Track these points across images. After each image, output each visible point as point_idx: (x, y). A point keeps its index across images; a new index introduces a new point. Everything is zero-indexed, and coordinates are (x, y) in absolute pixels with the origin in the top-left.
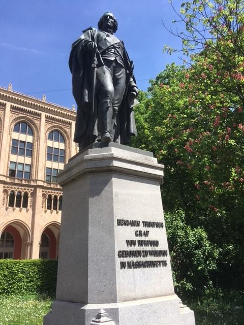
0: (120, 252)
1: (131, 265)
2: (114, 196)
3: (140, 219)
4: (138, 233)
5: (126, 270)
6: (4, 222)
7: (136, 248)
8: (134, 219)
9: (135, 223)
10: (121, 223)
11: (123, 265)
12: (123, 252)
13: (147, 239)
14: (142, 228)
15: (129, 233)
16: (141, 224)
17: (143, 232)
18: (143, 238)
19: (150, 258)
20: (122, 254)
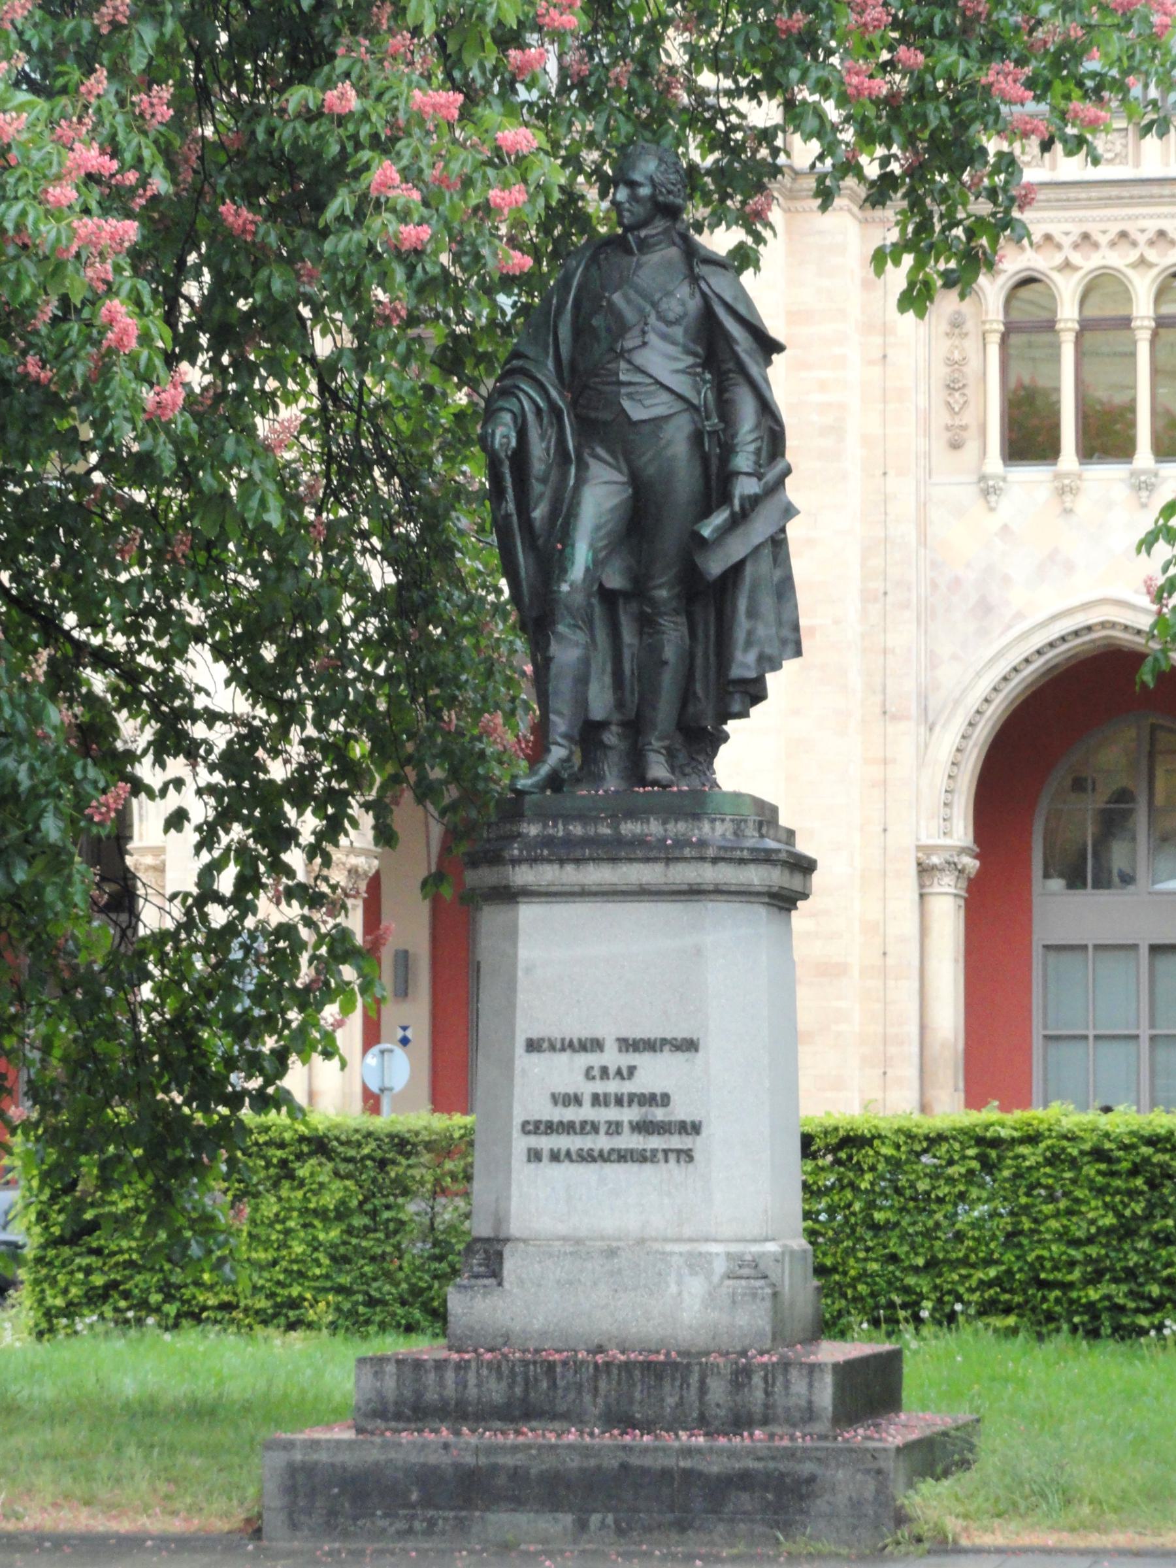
0: (526, 1123)
1: (555, 1157)
2: (520, 974)
3: (609, 1033)
4: (596, 1072)
5: (548, 1169)
6: (664, 1100)
7: (588, 1112)
8: (585, 1034)
9: (596, 1045)
10: (533, 1046)
11: (535, 1156)
12: (537, 1123)
13: (627, 1087)
14: (612, 1058)
15: (567, 1072)
16: (611, 1046)
17: (612, 1071)
18: (613, 1087)
19: (630, 1141)
20: (534, 1128)
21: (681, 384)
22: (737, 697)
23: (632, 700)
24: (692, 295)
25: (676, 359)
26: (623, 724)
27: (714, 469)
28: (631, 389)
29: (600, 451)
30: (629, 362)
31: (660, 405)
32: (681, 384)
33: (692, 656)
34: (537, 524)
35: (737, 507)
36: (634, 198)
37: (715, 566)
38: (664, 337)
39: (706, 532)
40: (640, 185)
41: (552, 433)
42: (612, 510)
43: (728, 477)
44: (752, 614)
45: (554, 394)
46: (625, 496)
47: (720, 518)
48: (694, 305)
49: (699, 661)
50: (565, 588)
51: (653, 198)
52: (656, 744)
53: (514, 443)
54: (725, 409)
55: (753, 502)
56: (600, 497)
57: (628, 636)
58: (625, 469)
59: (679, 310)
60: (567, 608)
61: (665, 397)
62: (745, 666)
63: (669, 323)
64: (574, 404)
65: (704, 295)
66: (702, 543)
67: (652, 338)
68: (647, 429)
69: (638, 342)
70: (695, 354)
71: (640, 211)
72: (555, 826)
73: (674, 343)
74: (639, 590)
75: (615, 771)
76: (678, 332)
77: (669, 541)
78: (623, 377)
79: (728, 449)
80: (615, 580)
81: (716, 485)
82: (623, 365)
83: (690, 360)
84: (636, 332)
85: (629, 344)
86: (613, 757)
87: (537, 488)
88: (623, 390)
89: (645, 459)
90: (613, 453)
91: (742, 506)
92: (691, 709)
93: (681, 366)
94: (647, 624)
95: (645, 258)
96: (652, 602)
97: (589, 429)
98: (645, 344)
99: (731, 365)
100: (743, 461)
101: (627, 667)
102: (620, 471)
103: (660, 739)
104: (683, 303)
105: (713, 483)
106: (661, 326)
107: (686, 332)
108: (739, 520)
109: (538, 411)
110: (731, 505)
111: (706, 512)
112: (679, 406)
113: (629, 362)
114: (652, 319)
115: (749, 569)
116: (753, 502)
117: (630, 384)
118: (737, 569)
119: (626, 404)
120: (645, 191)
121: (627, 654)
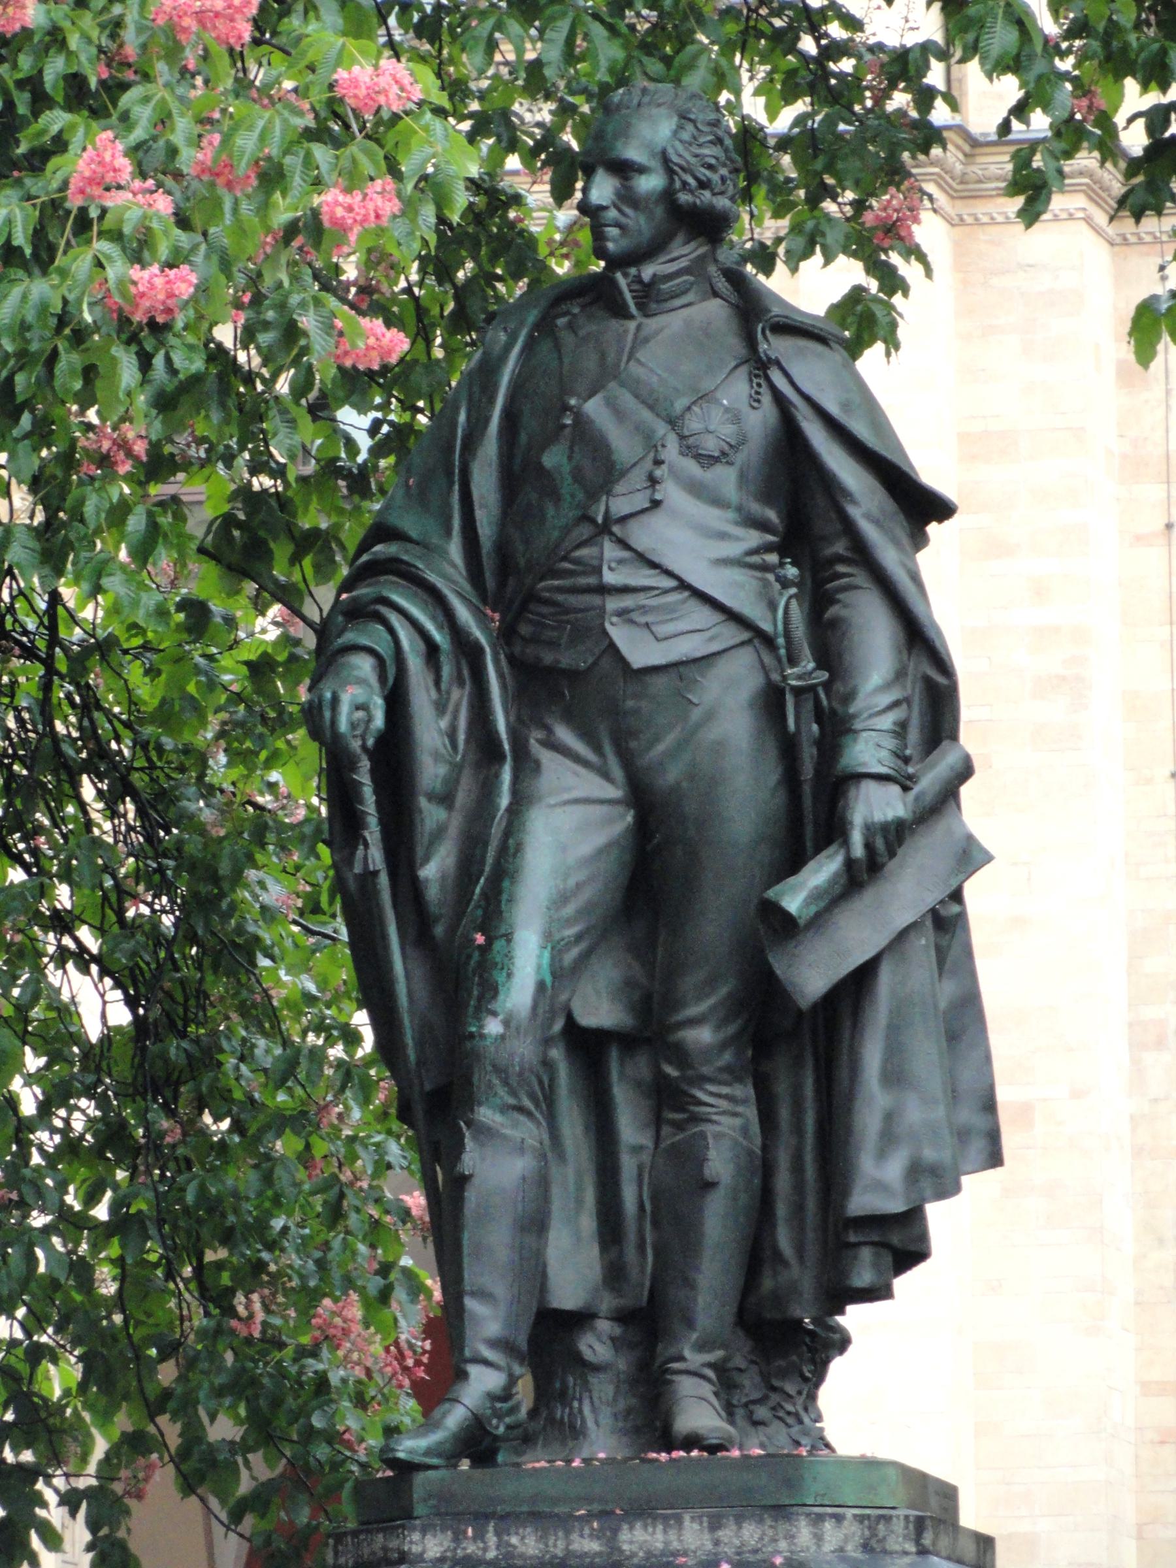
21: (737, 590)
22: (866, 1254)
23: (641, 1268)
24: (755, 400)
25: (723, 536)
26: (622, 1317)
27: (808, 770)
28: (628, 601)
29: (564, 734)
30: (624, 544)
31: (687, 635)
32: (737, 590)
33: (767, 1170)
34: (433, 893)
35: (858, 851)
36: (627, 198)
37: (812, 974)
38: (696, 490)
39: (795, 898)
40: (642, 170)
41: (460, 697)
42: (600, 852)
43: (837, 785)
44: (894, 1077)
45: (463, 614)
46: (599, 839)
47: (822, 871)
48: (761, 420)
49: (783, 1182)
50: (493, 1027)
51: (668, 196)
52: (694, 1359)
53: (379, 721)
54: (829, 641)
55: (894, 836)
56: (567, 830)
57: (631, 1128)
58: (617, 772)
59: (728, 431)
60: (497, 1069)
61: (702, 616)
62: (881, 1187)
63: (708, 460)
64: (506, 635)
65: (779, 398)
66: (785, 927)
67: (671, 492)
68: (659, 683)
69: (640, 501)
70: (762, 526)
71: (642, 224)
72: (480, 1536)
73: (717, 502)
74: (651, 1027)
75: (606, 1417)
76: (726, 479)
77: (714, 922)
78: (609, 578)
79: (836, 727)
80: (599, 1009)
81: (812, 807)
82: (610, 551)
83: (754, 538)
84: (637, 478)
85: (621, 505)
86: (603, 1387)
87: (431, 814)
88: (613, 604)
89: (661, 748)
90: (588, 736)
91: (869, 846)
92: (767, 1283)
93: (734, 549)
94: (669, 1100)
95: (652, 324)
96: (680, 1056)
97: (539, 688)
98: (656, 504)
99: (840, 547)
100: (869, 751)
101: (629, 1195)
102: (606, 775)
103: (702, 1346)
104: (735, 418)
105: (808, 802)
106: (691, 466)
107: (742, 477)
108: (859, 877)
109: (432, 651)
110: (846, 843)
111: (792, 861)
112: (732, 635)
113: (624, 544)
114: (671, 451)
115: (885, 978)
116: (894, 836)
117: (625, 590)
118: (862, 979)
119: (618, 633)
120: (650, 183)
121: (628, 1165)
